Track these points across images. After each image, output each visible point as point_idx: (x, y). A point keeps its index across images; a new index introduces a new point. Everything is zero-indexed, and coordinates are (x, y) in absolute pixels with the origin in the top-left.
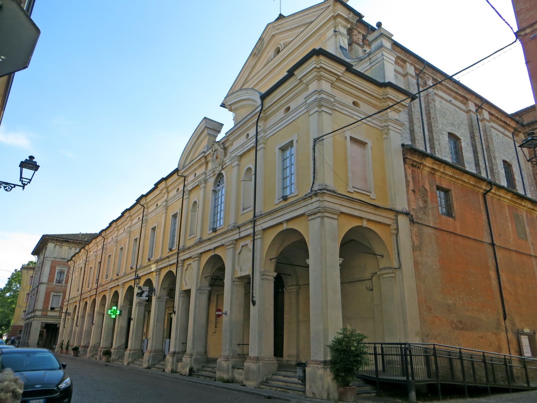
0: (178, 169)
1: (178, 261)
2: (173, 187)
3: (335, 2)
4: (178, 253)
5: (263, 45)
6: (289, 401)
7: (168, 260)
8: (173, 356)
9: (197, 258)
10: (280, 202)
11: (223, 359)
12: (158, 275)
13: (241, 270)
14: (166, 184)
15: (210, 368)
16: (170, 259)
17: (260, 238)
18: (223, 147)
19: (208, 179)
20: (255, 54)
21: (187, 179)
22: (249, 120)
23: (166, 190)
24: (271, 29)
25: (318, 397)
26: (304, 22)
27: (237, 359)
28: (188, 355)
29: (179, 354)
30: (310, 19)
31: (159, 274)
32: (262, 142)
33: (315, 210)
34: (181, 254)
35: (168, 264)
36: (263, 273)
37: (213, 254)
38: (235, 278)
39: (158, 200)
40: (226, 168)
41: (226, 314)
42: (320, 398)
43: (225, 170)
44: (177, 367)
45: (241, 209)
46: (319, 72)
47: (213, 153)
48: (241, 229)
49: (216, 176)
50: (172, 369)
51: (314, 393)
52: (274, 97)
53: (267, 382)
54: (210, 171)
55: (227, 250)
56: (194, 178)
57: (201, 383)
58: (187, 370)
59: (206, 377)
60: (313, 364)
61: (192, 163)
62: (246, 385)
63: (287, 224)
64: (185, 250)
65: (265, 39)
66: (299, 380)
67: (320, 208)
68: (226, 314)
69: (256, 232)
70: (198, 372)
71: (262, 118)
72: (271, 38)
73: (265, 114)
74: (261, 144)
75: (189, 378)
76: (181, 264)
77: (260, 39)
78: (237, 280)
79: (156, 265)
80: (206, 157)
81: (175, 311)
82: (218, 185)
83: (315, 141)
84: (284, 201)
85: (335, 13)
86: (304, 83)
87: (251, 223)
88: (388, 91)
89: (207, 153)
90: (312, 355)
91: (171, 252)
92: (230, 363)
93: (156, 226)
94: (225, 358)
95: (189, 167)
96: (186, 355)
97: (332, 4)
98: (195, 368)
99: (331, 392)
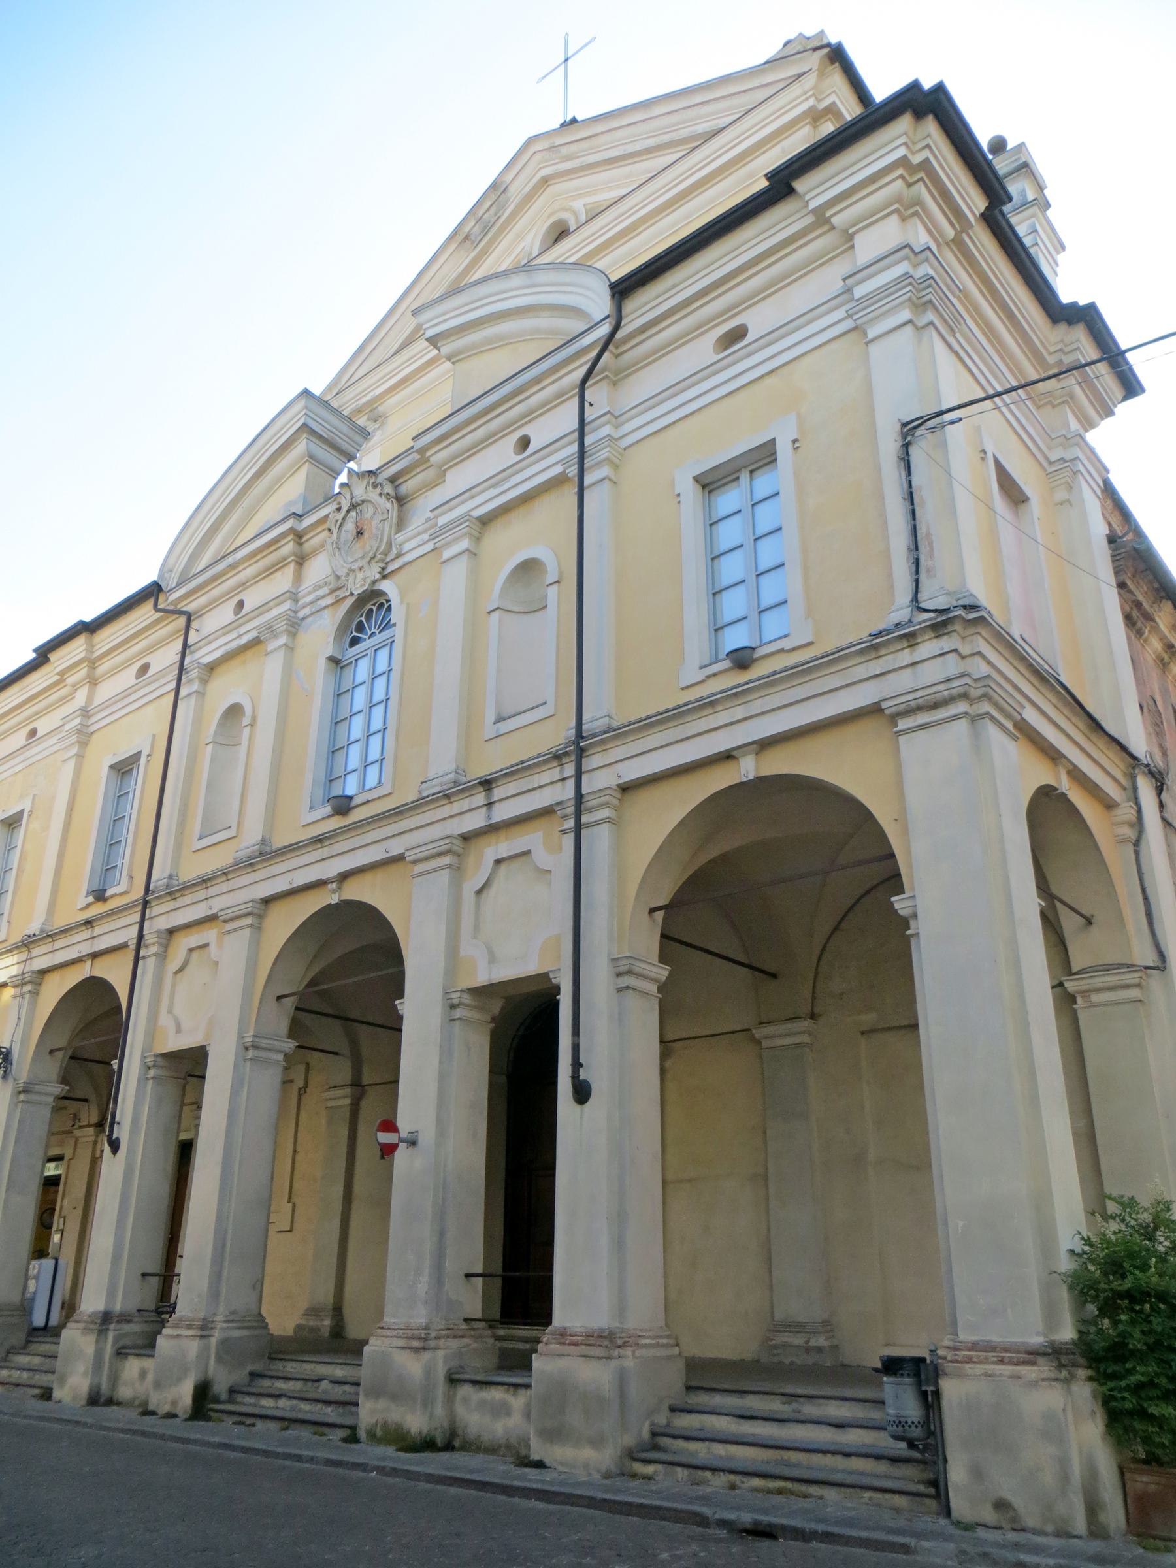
0: (160, 586)
1: (141, 936)
2: (119, 659)
3: (827, 62)
4: (146, 904)
5: (503, 207)
6: (905, 1549)
7: (86, 934)
8: (102, 1332)
9: (248, 921)
10: (708, 677)
11: (401, 1343)
12: (27, 996)
13: (492, 959)
14: (90, 648)
15: (292, 1383)
16: (97, 931)
17: (608, 820)
18: (392, 493)
19: (304, 619)
20: (467, 238)
21: (194, 625)
22: (537, 380)
23: (85, 670)
24: (538, 157)
25: (1030, 1522)
26: (684, 133)
27: (466, 1341)
28: (189, 1327)
29: (129, 1321)
30: (715, 122)
31: (35, 994)
32: (607, 459)
33: (941, 687)
34: (155, 910)
35: (86, 949)
36: (625, 962)
37: (334, 899)
38: (461, 991)
39: (38, 715)
40: (403, 572)
41: (413, 1143)
42: (1050, 1528)
43: (397, 578)
44: (114, 1379)
45: (490, 716)
46: (909, 185)
47: (340, 516)
48: (498, 793)
49: (350, 602)
50: (91, 1390)
51: (1001, 1505)
52: (674, 286)
53: (656, 1447)
54: (317, 587)
55: (415, 877)
56: (234, 618)
57: (299, 1458)
58: (185, 1393)
59: (288, 1422)
60: (986, 1361)
61: (230, 560)
62: (547, 1461)
63: (757, 761)
64: (175, 891)
65: (512, 189)
66: (897, 1438)
67: (966, 680)
68: (413, 1143)
69: (586, 799)
70: (231, 1401)
71: (604, 370)
72: (534, 188)
73: (617, 356)
74: (598, 464)
75: (200, 1431)
76: (154, 949)
77: (494, 186)
78: (467, 999)
79: (24, 956)
80: (299, 536)
81: (118, 1139)
82: (354, 642)
83: (909, 430)
84: (737, 671)
85: (819, 101)
86: (833, 228)
87: (555, 764)
88: (1078, 340)
89: (308, 521)
90: (388, 1309)
91: (100, 904)
92: (440, 1360)
93: (22, 812)
94: (413, 1338)
95: (215, 578)
96: (176, 1326)
97: (815, 67)
98: (220, 1387)
99: (1107, 1500)
